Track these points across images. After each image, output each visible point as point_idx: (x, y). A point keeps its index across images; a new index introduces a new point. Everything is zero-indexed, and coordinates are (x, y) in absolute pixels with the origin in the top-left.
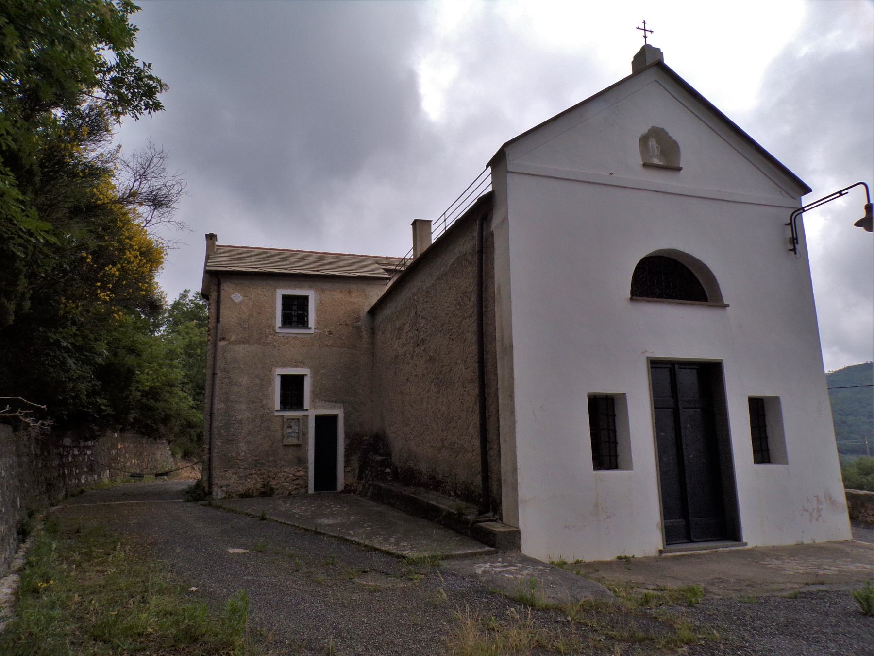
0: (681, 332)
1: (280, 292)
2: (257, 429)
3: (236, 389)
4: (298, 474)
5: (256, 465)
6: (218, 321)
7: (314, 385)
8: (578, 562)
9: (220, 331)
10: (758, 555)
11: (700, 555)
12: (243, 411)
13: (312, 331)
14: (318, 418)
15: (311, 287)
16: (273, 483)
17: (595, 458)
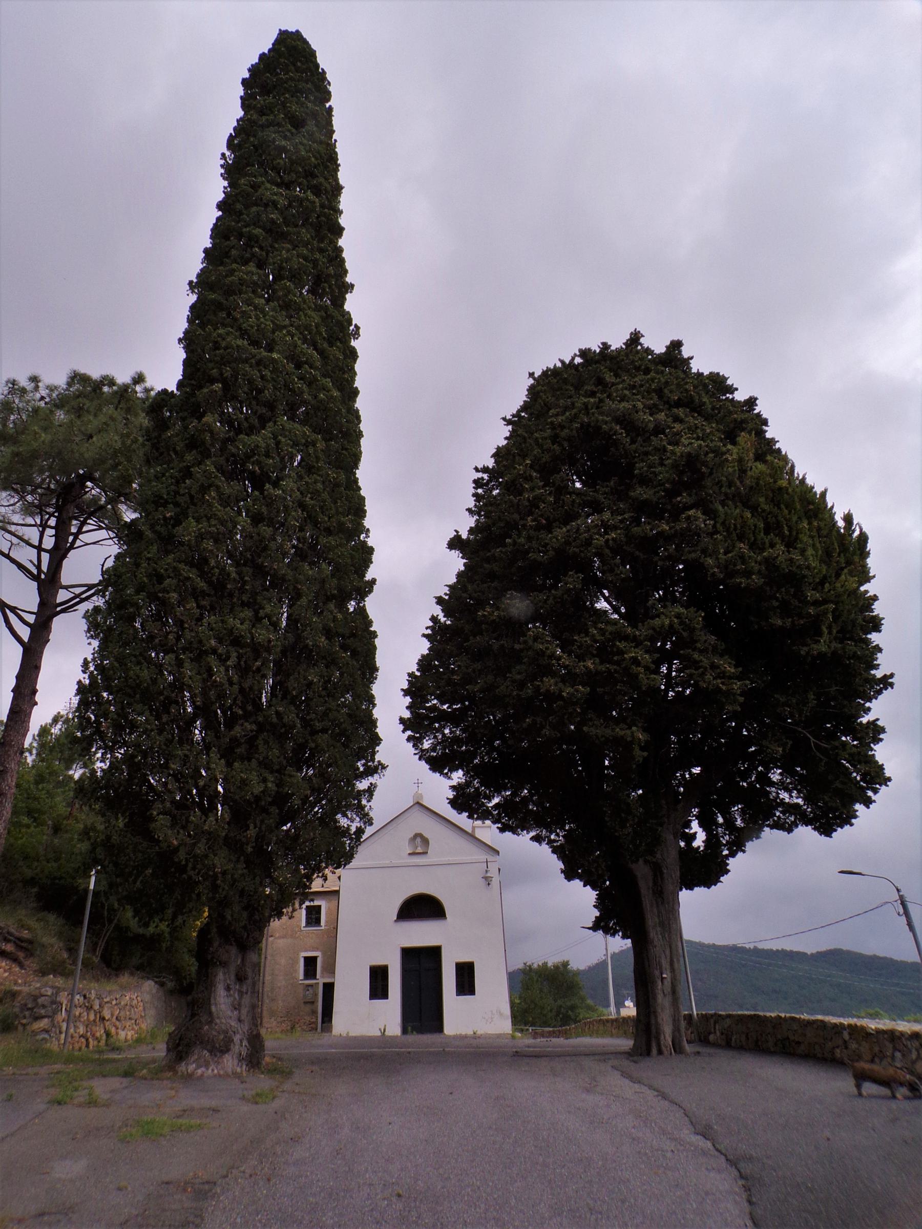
0: (421, 934)
7: (323, 962)
14: (325, 984)
15: (323, 899)
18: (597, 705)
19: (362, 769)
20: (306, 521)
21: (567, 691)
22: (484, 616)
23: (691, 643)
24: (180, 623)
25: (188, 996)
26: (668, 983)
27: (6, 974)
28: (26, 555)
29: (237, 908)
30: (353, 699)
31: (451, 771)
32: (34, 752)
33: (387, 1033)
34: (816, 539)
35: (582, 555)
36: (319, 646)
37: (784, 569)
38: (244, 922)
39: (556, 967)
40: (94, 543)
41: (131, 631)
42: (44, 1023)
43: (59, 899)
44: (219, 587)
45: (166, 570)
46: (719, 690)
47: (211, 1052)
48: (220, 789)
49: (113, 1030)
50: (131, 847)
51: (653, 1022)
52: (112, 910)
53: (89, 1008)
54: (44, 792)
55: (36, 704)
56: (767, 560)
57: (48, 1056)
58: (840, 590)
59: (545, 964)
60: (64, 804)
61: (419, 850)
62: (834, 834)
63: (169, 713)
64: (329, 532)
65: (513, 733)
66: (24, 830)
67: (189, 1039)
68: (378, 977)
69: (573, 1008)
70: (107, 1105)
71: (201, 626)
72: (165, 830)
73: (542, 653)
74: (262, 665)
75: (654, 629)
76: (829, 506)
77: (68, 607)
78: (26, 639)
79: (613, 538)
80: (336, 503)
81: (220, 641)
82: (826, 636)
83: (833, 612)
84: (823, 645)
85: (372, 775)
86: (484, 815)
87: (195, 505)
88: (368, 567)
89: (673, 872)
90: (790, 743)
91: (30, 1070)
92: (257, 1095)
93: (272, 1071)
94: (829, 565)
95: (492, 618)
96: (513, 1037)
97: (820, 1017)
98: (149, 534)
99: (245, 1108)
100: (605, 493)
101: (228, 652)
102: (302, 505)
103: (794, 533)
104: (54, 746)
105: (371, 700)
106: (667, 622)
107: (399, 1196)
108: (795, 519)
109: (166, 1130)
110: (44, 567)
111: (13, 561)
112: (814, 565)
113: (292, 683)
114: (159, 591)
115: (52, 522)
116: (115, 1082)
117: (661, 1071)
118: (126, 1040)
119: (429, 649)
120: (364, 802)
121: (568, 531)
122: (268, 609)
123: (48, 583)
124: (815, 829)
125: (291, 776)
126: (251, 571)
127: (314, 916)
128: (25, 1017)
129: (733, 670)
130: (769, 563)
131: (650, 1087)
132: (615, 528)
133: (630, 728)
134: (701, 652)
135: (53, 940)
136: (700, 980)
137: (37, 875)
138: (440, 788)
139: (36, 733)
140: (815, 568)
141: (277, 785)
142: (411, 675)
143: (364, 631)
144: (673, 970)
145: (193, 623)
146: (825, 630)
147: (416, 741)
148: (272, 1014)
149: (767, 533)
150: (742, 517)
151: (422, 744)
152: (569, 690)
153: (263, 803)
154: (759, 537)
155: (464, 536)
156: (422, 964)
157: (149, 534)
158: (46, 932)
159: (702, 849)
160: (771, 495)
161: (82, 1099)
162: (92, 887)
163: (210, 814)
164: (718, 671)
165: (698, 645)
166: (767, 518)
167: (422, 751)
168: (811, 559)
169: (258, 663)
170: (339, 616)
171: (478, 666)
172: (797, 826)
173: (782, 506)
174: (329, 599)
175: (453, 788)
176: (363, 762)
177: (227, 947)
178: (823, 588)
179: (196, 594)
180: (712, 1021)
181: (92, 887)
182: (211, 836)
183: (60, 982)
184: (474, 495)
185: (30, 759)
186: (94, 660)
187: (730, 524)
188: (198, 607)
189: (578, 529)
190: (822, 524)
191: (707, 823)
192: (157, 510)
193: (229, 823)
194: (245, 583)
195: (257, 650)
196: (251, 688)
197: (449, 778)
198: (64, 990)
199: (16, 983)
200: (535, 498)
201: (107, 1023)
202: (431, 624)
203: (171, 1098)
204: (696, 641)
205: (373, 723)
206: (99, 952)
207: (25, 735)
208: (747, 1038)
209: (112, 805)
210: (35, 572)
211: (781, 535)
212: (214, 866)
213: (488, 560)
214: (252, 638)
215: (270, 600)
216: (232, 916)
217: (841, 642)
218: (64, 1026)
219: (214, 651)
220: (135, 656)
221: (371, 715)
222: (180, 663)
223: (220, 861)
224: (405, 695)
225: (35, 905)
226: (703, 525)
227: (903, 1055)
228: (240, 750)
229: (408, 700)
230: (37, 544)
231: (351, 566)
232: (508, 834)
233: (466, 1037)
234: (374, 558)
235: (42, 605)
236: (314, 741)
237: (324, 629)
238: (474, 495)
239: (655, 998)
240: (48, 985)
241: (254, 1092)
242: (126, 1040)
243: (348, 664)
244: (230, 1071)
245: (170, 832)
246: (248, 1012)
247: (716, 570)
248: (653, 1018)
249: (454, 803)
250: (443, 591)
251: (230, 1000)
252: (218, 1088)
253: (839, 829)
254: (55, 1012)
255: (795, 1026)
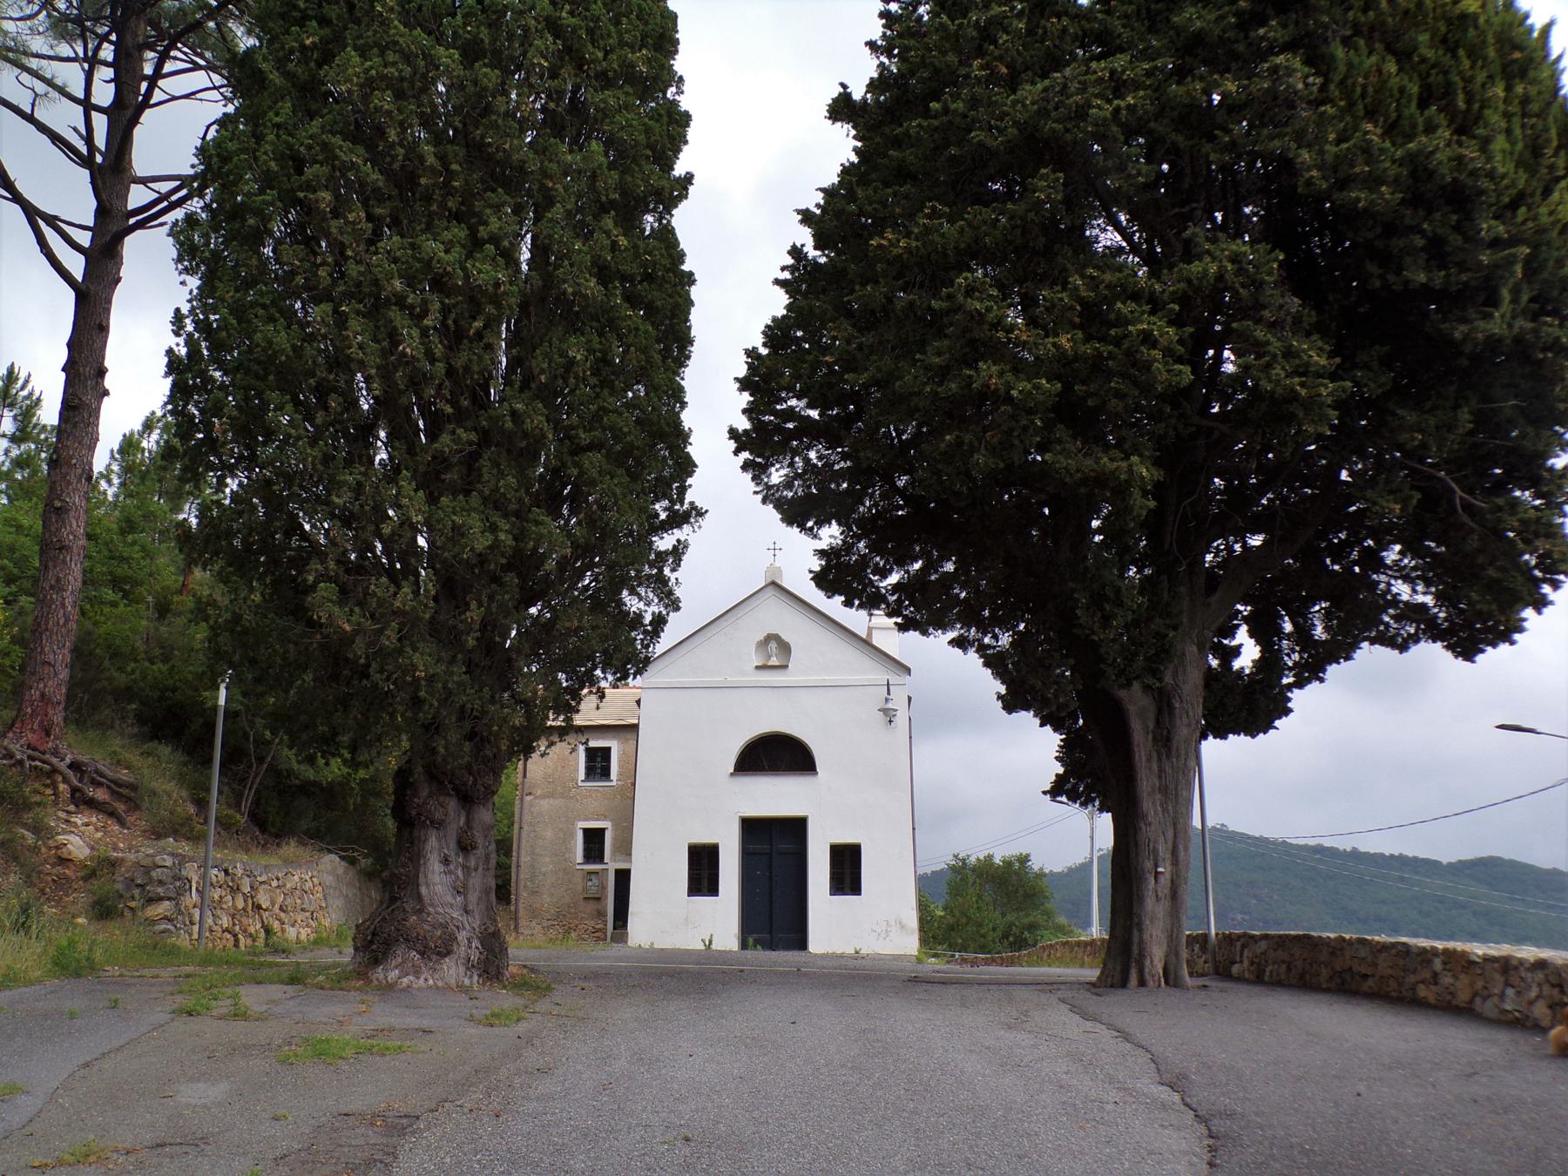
0: (775, 796)
3: (541, 842)
7: (615, 839)
12: (547, 865)
18: (1073, 417)
19: (663, 516)
20: (562, 59)
21: (1019, 388)
22: (880, 246)
23: (1252, 310)
24: (339, 248)
25: (389, 876)
26: (1165, 881)
27: (99, 835)
28: (65, 117)
29: (454, 736)
30: (647, 394)
31: (819, 524)
32: (116, 481)
33: (714, 947)
34: (1516, 121)
35: (1068, 137)
36: (585, 296)
37: (1443, 176)
38: (467, 759)
39: (1008, 863)
40: (187, 96)
41: (254, 262)
42: (164, 908)
43: (172, 721)
44: (405, 180)
45: (310, 148)
46: (1293, 396)
47: (422, 954)
48: (421, 542)
49: (276, 925)
50: (275, 634)
51: (1136, 939)
52: (261, 743)
53: (234, 890)
54: (137, 548)
55: (106, 393)
56: (1411, 158)
57: (173, 953)
58: (1545, 220)
59: (990, 857)
60: (172, 569)
61: (774, 661)
62: (1480, 658)
63: (326, 408)
64: (605, 81)
65: (928, 459)
66: (107, 610)
67: (386, 934)
69: (1032, 927)
70: (261, 1018)
71: (376, 253)
72: (325, 602)
73: (979, 318)
74: (485, 327)
75: (1189, 281)
76: (1554, 56)
77: (147, 218)
78: (79, 276)
79: (1129, 107)
80: (617, 23)
81: (411, 281)
82: (1506, 306)
83: (1528, 261)
84: (1497, 323)
85: (679, 526)
86: (872, 601)
87: (358, 22)
88: (679, 150)
89: (1191, 703)
90: (1418, 496)
91: (146, 972)
92: (493, 1015)
93: (520, 985)
94: (1532, 171)
95: (895, 251)
96: (919, 961)
97: (1404, 939)
98: (275, 77)
99: (473, 1031)
100: (1126, 16)
101: (425, 302)
102: (553, 26)
103: (1476, 106)
104: (148, 471)
105: (678, 395)
106: (1213, 268)
107: (687, 1139)
108: (1481, 77)
109: (349, 1052)
110: (100, 140)
111: (42, 128)
112: (1501, 170)
113: (539, 363)
114: (301, 188)
115: (107, 52)
116: (276, 991)
117: (1133, 1011)
118: (298, 941)
119: (789, 307)
120: (667, 571)
121: (1045, 90)
122: (495, 224)
123: (109, 170)
124: (1447, 647)
125: (538, 523)
126: (462, 152)
127: (598, 763)
128: (133, 898)
129: (1323, 362)
130: (1418, 168)
131: (1110, 1026)
132: (1136, 85)
133: (1127, 458)
134: (1273, 326)
135: (171, 786)
136: (1255, 896)
137: (134, 681)
138: (799, 553)
139: (116, 448)
140: (1503, 177)
141: (515, 539)
142: (751, 353)
143: (668, 271)
144: (1175, 862)
145: (362, 247)
146: (1506, 294)
147: (756, 470)
148: (534, 914)
149: (1423, 104)
150: (1380, 72)
151: (769, 476)
152: (1024, 385)
153: (492, 567)
154: (1407, 112)
155: (858, 93)
156: (775, 846)
157: (275, 77)
158: (158, 772)
159: (1247, 671)
160: (1443, 29)
161: (224, 1011)
162: (222, 702)
163: (404, 583)
164: (1297, 361)
165: (1266, 313)
166: (1428, 75)
167: (768, 487)
168: (1499, 157)
169: (478, 324)
170: (623, 241)
171: (868, 339)
172: (1417, 641)
173: (1461, 52)
174: (604, 209)
175: (821, 553)
176: (666, 503)
177: (441, 799)
178: (1514, 216)
179: (369, 196)
180: (1239, 944)
181: (222, 702)
182: (408, 621)
183: (185, 848)
184: (882, 15)
185: (110, 491)
186: (192, 311)
187: (1354, 84)
188: (370, 218)
189: (1065, 86)
190: (1533, 90)
191: (1264, 632)
192: (287, 32)
193: (435, 599)
194: (451, 176)
195: (475, 299)
196: (467, 369)
197: (815, 537)
198: (192, 860)
199: (115, 849)
200: (989, 22)
201: (265, 915)
202: (790, 261)
203: (360, 1014)
204: (1264, 307)
205: (682, 436)
206: (246, 805)
207: (92, 448)
208: (1289, 969)
209: (239, 565)
210: (84, 150)
211: (1449, 110)
212: (415, 667)
213: (897, 143)
214: (467, 277)
215: (498, 208)
216: (446, 749)
217: (1535, 317)
218: (196, 913)
219: (400, 301)
220: (264, 307)
221: (678, 423)
222: (341, 320)
223: (423, 660)
224: (741, 390)
225: (136, 730)
226: (1300, 86)
227: (1519, 993)
228: (451, 476)
229: (746, 397)
230: (81, 95)
231: (642, 147)
232: (913, 635)
233: (842, 956)
234: (692, 133)
235: (102, 212)
236: (577, 465)
237: (594, 263)
238: (882, 15)
239: (1141, 900)
240: (165, 853)
241: (488, 1012)
242: (298, 941)
243: (637, 329)
244: (453, 982)
245: (336, 609)
246: (479, 898)
247: (1314, 173)
248: (1136, 933)
249: (820, 579)
250: (813, 201)
251: (449, 879)
252: (432, 1006)
253: (1489, 649)
254: (180, 892)
255: (1363, 953)
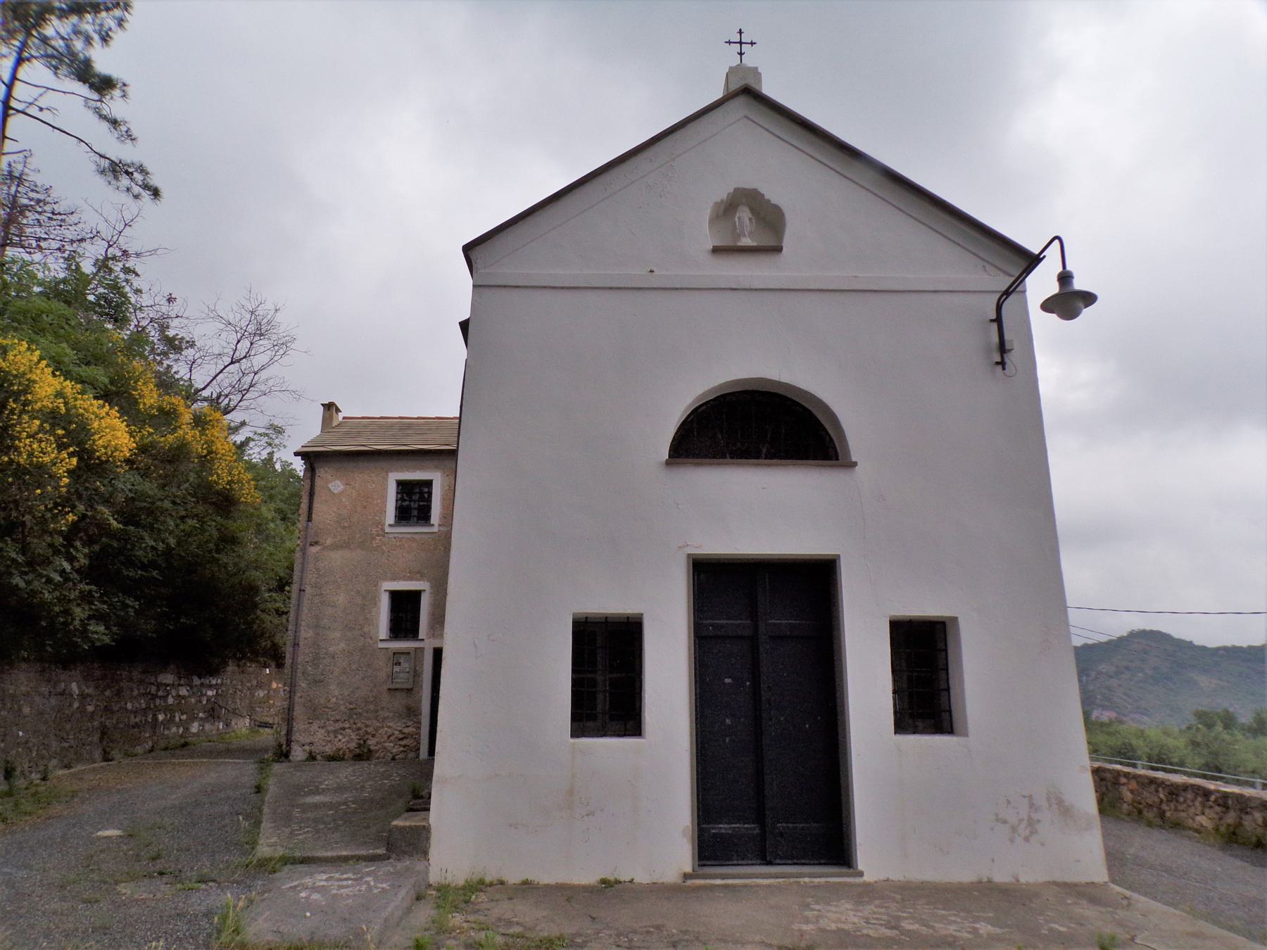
0: (763, 513)
1: (394, 477)
2: (354, 667)
4: (406, 730)
5: (350, 717)
6: (309, 519)
8: (526, 883)
9: (311, 532)
10: (869, 892)
11: (734, 886)
12: (336, 642)
13: (435, 529)
16: (372, 742)
17: (575, 718)
68: (925, 691)
